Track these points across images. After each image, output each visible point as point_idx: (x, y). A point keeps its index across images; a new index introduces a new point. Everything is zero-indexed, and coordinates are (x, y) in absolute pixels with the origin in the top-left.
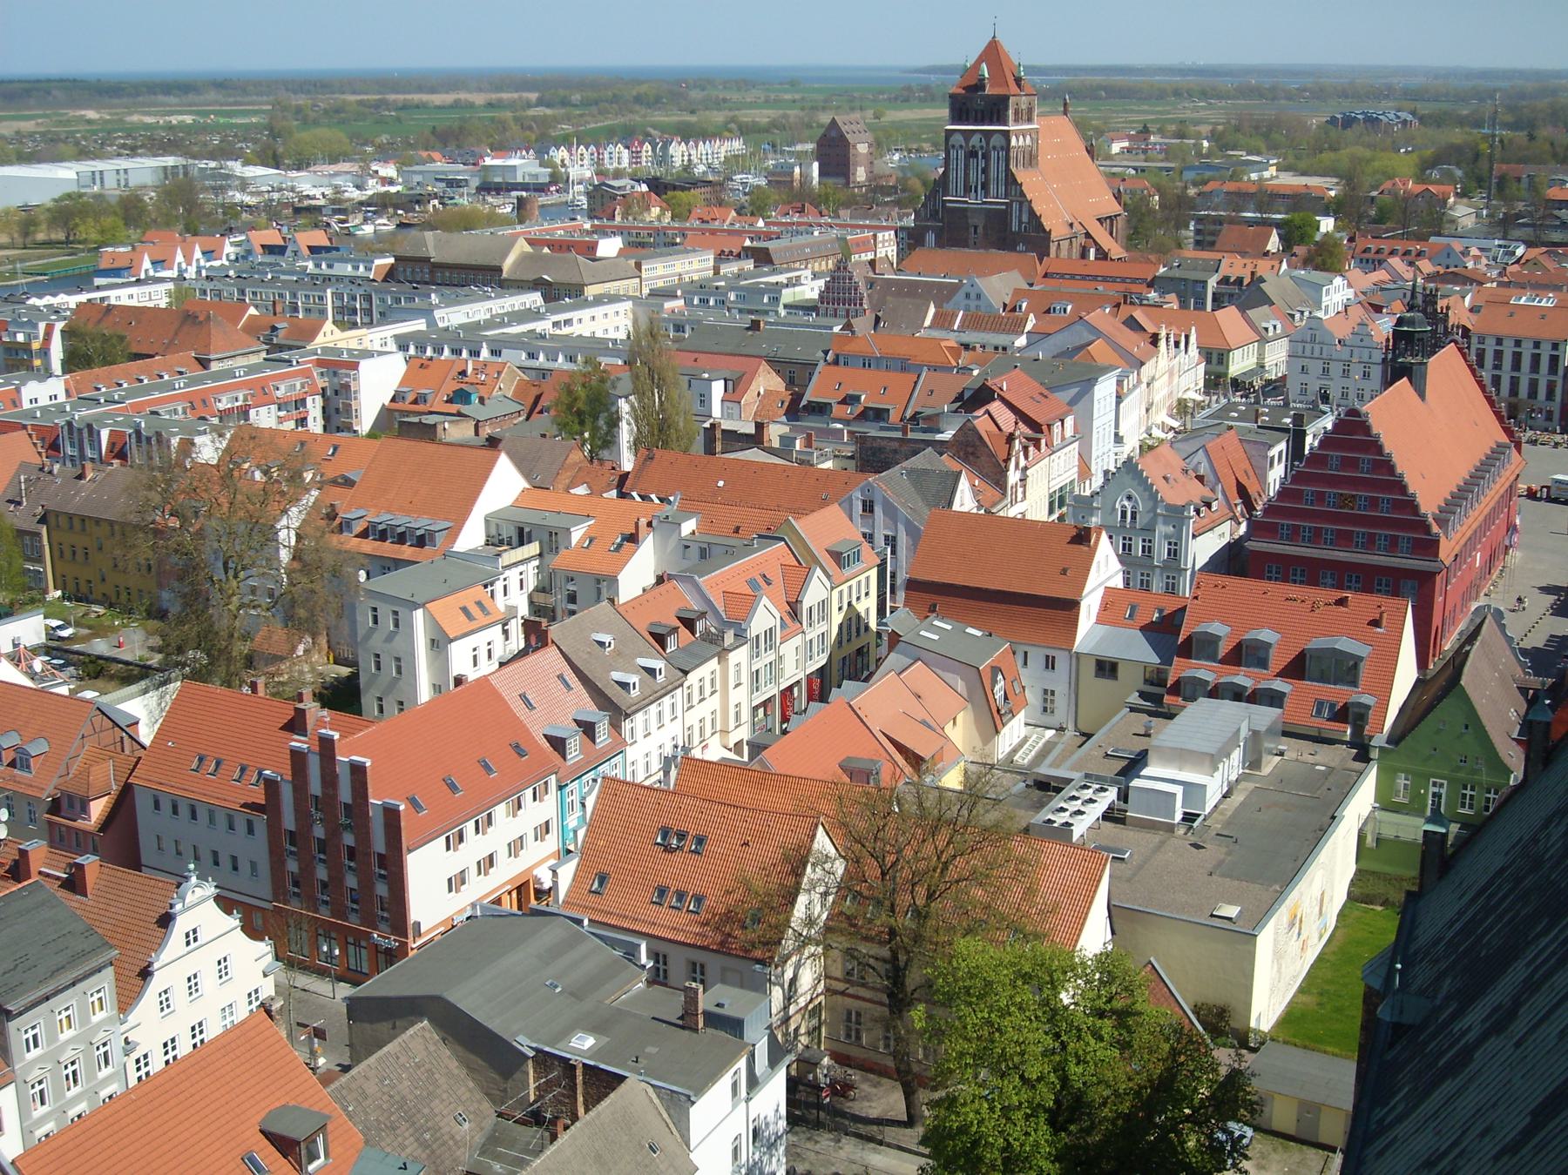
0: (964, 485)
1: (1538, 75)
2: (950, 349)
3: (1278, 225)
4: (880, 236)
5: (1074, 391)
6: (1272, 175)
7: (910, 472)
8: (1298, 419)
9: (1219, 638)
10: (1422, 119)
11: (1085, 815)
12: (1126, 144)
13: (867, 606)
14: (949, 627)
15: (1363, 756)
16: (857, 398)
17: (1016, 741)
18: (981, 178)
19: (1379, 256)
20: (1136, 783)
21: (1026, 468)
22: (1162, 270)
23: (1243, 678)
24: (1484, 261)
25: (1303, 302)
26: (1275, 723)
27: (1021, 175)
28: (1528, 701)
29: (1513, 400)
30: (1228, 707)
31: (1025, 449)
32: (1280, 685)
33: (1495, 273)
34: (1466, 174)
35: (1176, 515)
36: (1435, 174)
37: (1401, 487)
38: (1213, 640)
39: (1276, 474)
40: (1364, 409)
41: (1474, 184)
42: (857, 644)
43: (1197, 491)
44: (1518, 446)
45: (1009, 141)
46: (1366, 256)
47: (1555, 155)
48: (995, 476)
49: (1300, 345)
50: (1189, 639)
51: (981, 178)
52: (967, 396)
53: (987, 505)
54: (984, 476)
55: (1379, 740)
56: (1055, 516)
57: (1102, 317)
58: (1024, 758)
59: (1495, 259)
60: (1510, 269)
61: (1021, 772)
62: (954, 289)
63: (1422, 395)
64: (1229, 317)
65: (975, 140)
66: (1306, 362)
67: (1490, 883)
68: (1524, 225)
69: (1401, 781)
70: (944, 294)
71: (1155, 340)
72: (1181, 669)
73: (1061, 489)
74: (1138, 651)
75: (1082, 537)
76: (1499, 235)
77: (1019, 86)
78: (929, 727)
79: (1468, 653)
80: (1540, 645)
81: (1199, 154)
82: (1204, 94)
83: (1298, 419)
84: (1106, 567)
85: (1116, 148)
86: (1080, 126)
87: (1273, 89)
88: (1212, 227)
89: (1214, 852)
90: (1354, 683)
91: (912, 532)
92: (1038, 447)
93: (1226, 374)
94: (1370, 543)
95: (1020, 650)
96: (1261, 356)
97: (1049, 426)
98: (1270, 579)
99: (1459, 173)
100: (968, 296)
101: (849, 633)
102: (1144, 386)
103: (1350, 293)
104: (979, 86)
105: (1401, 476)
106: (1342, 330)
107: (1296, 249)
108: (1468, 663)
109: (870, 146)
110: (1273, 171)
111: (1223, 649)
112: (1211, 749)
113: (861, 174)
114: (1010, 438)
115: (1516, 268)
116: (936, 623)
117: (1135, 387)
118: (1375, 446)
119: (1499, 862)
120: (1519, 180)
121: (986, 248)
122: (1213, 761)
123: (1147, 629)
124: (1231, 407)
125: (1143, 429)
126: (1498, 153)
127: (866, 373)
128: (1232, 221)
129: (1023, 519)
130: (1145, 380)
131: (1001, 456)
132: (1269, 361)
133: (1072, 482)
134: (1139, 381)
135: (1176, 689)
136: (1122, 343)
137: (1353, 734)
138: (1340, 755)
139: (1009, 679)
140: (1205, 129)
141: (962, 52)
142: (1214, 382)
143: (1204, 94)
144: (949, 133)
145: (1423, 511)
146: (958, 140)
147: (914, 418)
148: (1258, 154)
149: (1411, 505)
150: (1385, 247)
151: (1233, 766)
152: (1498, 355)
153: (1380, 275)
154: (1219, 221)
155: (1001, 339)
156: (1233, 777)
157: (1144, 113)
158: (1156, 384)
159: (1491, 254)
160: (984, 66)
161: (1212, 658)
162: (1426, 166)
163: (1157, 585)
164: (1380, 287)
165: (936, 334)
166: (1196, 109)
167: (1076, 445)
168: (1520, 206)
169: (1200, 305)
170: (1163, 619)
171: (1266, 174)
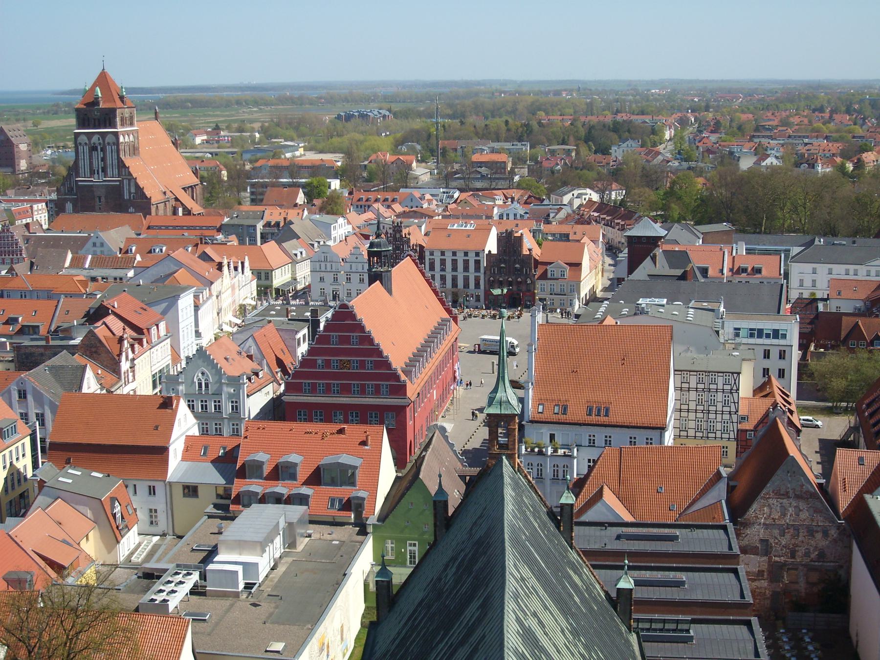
0: (89, 374)
1: (467, 84)
2: (80, 281)
3: (303, 186)
4: (35, 207)
5: (164, 305)
6: (301, 154)
7: (51, 368)
8: (314, 313)
9: (263, 463)
10: (396, 115)
11: (176, 594)
12: (205, 137)
13: (25, 464)
14: (79, 473)
15: (363, 532)
16: (16, 320)
17: (132, 547)
18: (101, 164)
20: (211, 567)
21: (133, 360)
22: (226, 220)
23: (281, 488)
24: (435, 202)
25: (320, 236)
26: (303, 516)
27: (128, 161)
28: (466, 483)
29: (454, 290)
30: (271, 509)
31: (132, 346)
32: (306, 490)
33: (440, 210)
34: (423, 147)
35: (235, 381)
36: (404, 149)
37: (378, 352)
38: (259, 465)
39: (303, 348)
40: (350, 304)
41: (429, 154)
42: (19, 490)
43: (249, 366)
44: (455, 319)
45: (118, 139)
47: (477, 134)
48: (110, 364)
49: (318, 264)
50: (243, 465)
51: (101, 164)
52: (92, 312)
53: (107, 387)
54: (105, 367)
55: (372, 520)
56: (157, 390)
57: (185, 255)
58: (137, 558)
59: (441, 201)
60: (449, 207)
61: (135, 567)
62: (85, 240)
63: (390, 291)
64: (271, 249)
65: (95, 139)
66: (322, 274)
67: (415, 611)
68: (458, 178)
69: (389, 545)
70: (77, 245)
71: (220, 267)
72: (239, 486)
75: (167, 404)
76: (444, 186)
77: (123, 102)
78: (68, 544)
79: (424, 456)
80: (478, 446)
81: (254, 142)
82: (256, 103)
83: (314, 313)
84: (185, 424)
85: (198, 140)
86: (170, 129)
87: (301, 98)
88: (261, 190)
89: (266, 607)
90: (353, 484)
91: (54, 409)
92: (141, 344)
93: (271, 286)
94: (363, 391)
95: (130, 484)
96: (294, 272)
97: (148, 330)
99: (419, 147)
101: (13, 485)
102: (214, 298)
103: (349, 228)
104: (96, 102)
105: (378, 345)
106: (344, 252)
107: (315, 202)
108: (424, 464)
109: (29, 145)
110: (301, 151)
111: (266, 470)
112: (260, 537)
113: (23, 165)
114: (121, 340)
115: (454, 206)
116: (70, 471)
119: (421, 595)
120: (456, 150)
121: (108, 211)
122: (262, 546)
123: (216, 462)
124: (271, 307)
125: (217, 326)
126: (441, 134)
127: (24, 302)
128: (273, 185)
129: (135, 395)
130: (215, 294)
131: (116, 352)
132: (299, 275)
134: (211, 295)
135: (238, 500)
136: (198, 270)
137: (355, 517)
138: (348, 532)
139: (124, 505)
140: (257, 126)
141: (85, 80)
142: (263, 291)
143: (256, 103)
144: (77, 135)
145: (394, 366)
146: (83, 139)
147: (56, 331)
148: (292, 140)
149: (387, 364)
150: (372, 196)
151: (277, 546)
153: (369, 215)
154: (265, 185)
155: (118, 273)
156: (277, 555)
157: (218, 116)
158: (223, 296)
159: (438, 198)
160: (98, 89)
161: (261, 477)
162: (399, 143)
163: (226, 431)
164: (368, 223)
165: (73, 272)
166: (252, 113)
167: (168, 341)
168: (456, 167)
169: (253, 241)
170: (226, 453)
171: (297, 153)
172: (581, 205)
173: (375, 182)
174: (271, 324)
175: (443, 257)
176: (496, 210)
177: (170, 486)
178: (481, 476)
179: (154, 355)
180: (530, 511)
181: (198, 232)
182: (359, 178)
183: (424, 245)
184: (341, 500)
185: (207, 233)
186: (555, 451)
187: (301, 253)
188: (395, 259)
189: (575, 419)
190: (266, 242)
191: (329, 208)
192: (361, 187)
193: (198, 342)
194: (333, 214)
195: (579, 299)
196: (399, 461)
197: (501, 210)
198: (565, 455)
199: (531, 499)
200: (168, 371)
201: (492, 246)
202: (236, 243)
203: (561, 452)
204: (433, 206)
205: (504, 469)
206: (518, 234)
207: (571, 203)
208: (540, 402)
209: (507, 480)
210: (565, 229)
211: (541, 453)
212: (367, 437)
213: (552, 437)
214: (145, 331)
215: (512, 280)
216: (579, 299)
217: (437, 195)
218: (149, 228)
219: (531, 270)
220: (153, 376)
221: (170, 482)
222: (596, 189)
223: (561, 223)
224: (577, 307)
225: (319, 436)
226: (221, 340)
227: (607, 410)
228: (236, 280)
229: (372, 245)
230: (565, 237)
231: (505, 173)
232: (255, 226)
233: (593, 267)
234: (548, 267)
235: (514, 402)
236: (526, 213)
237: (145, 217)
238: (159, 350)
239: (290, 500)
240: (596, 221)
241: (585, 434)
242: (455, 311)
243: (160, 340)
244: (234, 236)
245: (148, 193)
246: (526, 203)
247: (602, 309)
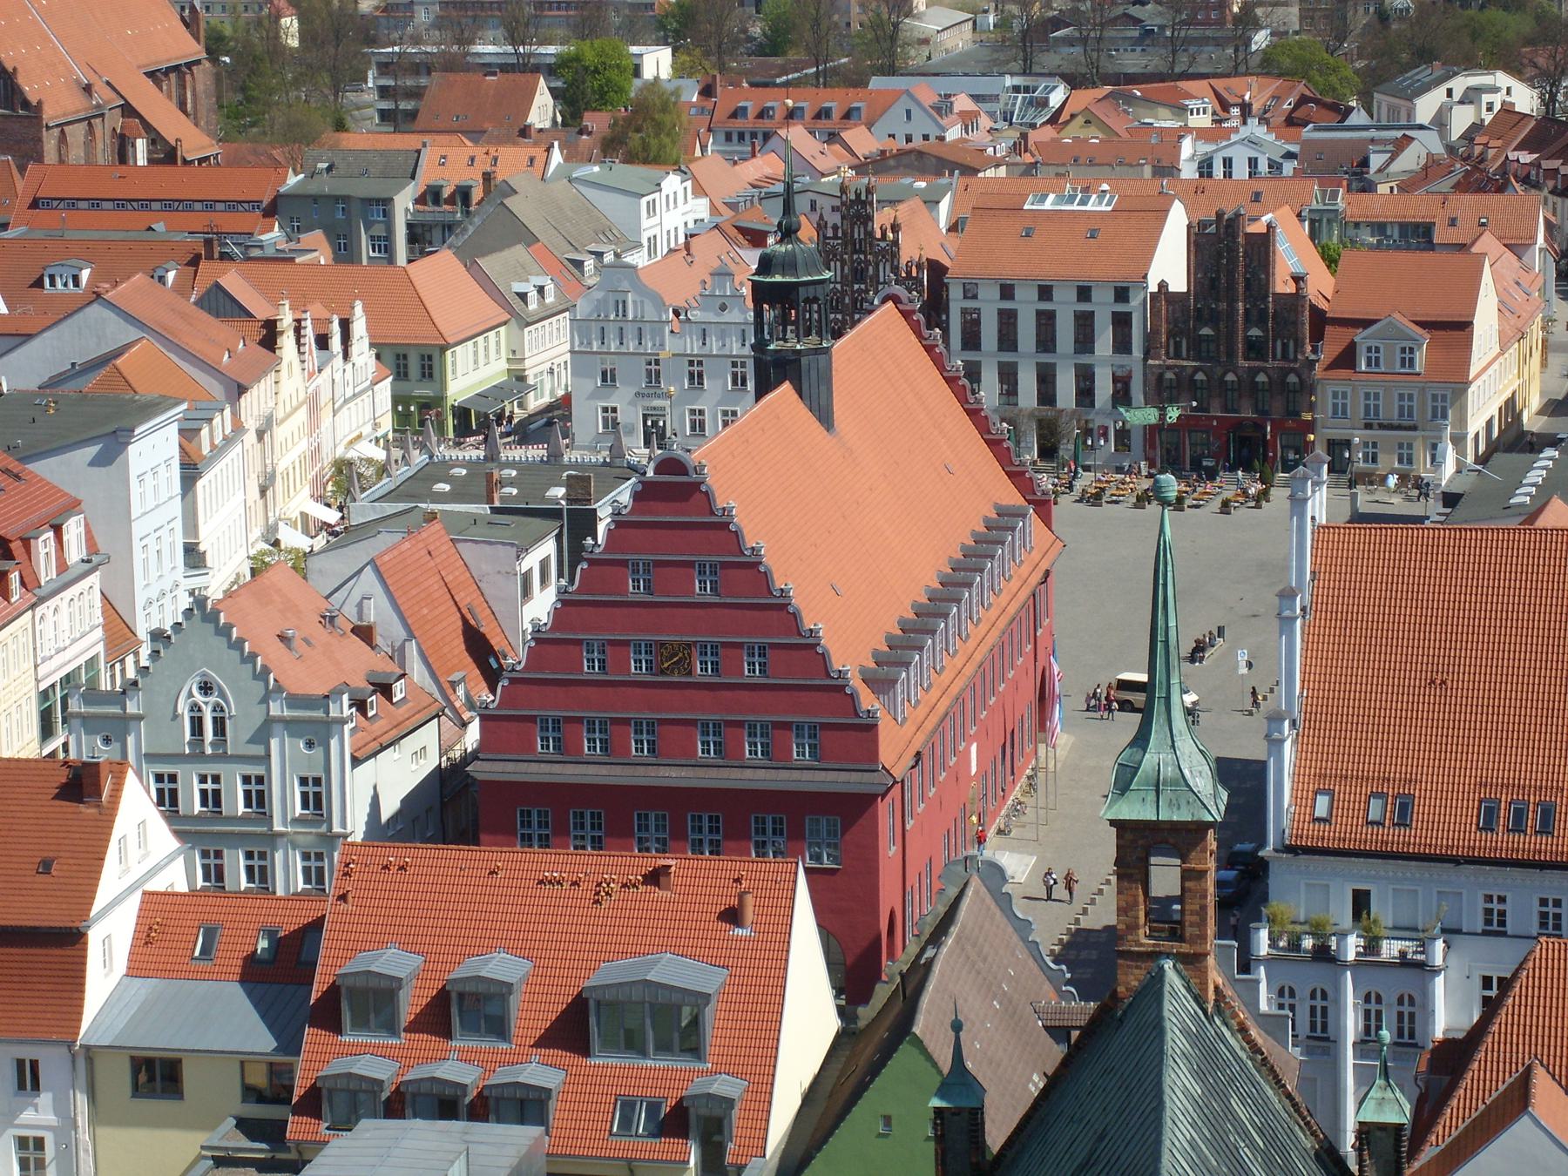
19: (766, 124)
22: (293, 180)
23: (459, 1065)
24: (985, 122)
26: (527, 1158)
29: (1046, 411)
33: (1002, 149)
40: (694, 458)
43: (358, 663)
44: (1043, 507)
46: (739, 124)
50: (333, 992)
59: (1007, 117)
60: (1034, 136)
63: (825, 417)
64: (439, 278)
71: (269, 337)
72: (325, 1057)
73: (67, 679)
74: (229, 1024)
75: (82, 786)
79: (930, 964)
83: (580, 487)
84: (142, 853)
90: (694, 1049)
93: (440, 399)
97: (26, 543)
98: (527, 840)
102: (250, 438)
103: (700, 208)
108: (931, 987)
111: (409, 1005)
115: (1048, 133)
117: (229, 441)
118: (722, 529)
123: (255, 974)
124: (436, 470)
125: (257, 532)
128: (452, 65)
130: (251, 424)
132: (534, 367)
133: (91, 663)
134: (238, 428)
135: (312, 1104)
142: (418, 411)
145: (837, 664)
149: (809, 650)
152: (1008, 320)
153: (766, 165)
154: (423, 67)
158: (280, 433)
159: (997, 108)
161: (391, 1028)
167: (94, 579)
169: (384, 245)
170: (280, 945)
172: (1476, 128)
173: (792, 55)
174: (436, 526)
175: (1007, 305)
176: (1187, 147)
177: (90, 1060)
178: (1095, 1028)
179: (47, 629)
180: (1252, 1144)
181: (199, 220)
182: (736, 42)
183: (946, 262)
184: (653, 1108)
185: (225, 221)
186: (1372, 946)
187: (541, 290)
188: (845, 310)
189: (1439, 841)
190: (424, 254)
191: (635, 139)
192: (745, 73)
193: (196, 582)
194: (646, 162)
195: (1458, 441)
196: (853, 977)
197: (1205, 148)
198: (1404, 962)
199: (1262, 1106)
200: (93, 681)
201: (1170, 266)
202: (323, 257)
203: (1390, 949)
204: (979, 136)
205: (1168, 1006)
206: (1258, 228)
207: (1440, 122)
208: (1318, 781)
209: (1176, 1041)
210: (1417, 208)
211: (1323, 954)
212: (741, 896)
213: (1361, 902)
214: (16, 546)
215: (1238, 383)
216: (1458, 441)
217: (995, 98)
218: (34, 204)
219: (1299, 345)
220: (44, 695)
221: (87, 1048)
222: (1530, 71)
223: (1408, 185)
224: (1449, 468)
225: (587, 888)
226: (268, 577)
227: (1548, 815)
228: (323, 379)
229: (766, 265)
230: (1419, 235)
231: (1221, 22)
232: (386, 203)
233: (1511, 335)
234: (1360, 336)
235: (1202, 780)
236: (1290, 156)
237: (22, 169)
238: (64, 606)
239: (483, 1107)
240: (1526, 181)
241: (1470, 894)
242: (1046, 482)
243: (67, 577)
244: (318, 234)
245: (30, 89)
246: (1292, 121)
247: (1536, 476)
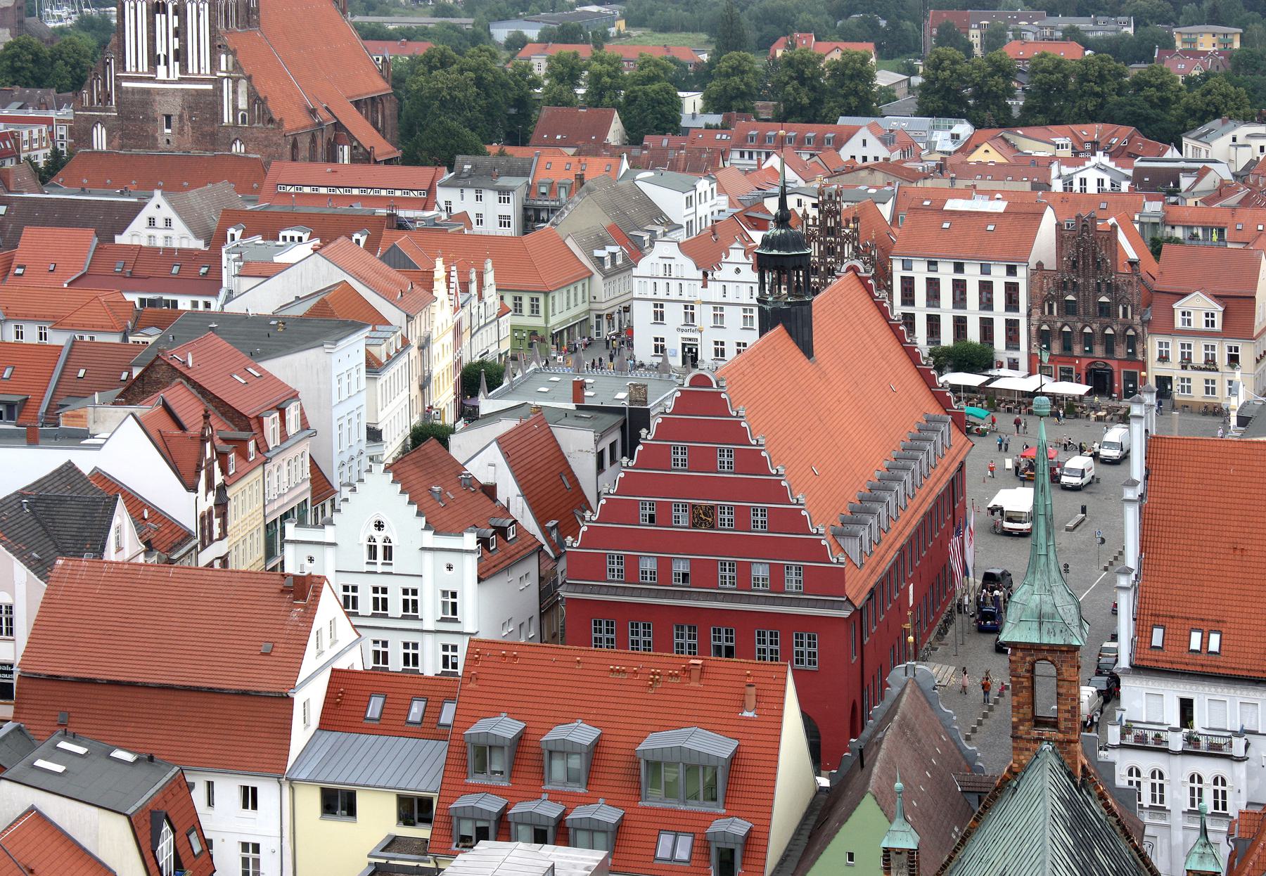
14: (81, 750)
31: (222, 457)
63: (807, 350)
92: (243, 455)
100: (152, 222)
102: (414, 352)
116: (63, 745)
